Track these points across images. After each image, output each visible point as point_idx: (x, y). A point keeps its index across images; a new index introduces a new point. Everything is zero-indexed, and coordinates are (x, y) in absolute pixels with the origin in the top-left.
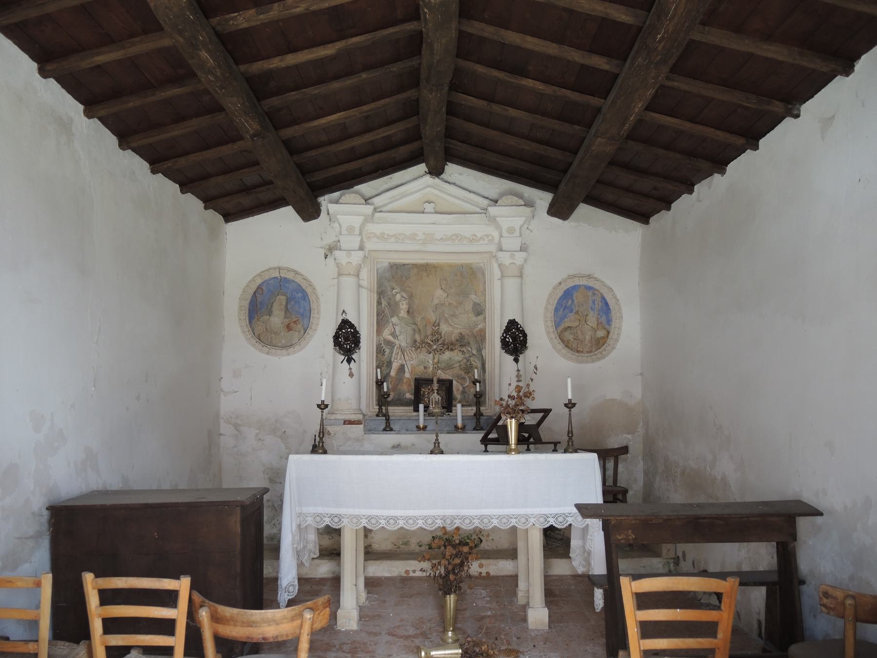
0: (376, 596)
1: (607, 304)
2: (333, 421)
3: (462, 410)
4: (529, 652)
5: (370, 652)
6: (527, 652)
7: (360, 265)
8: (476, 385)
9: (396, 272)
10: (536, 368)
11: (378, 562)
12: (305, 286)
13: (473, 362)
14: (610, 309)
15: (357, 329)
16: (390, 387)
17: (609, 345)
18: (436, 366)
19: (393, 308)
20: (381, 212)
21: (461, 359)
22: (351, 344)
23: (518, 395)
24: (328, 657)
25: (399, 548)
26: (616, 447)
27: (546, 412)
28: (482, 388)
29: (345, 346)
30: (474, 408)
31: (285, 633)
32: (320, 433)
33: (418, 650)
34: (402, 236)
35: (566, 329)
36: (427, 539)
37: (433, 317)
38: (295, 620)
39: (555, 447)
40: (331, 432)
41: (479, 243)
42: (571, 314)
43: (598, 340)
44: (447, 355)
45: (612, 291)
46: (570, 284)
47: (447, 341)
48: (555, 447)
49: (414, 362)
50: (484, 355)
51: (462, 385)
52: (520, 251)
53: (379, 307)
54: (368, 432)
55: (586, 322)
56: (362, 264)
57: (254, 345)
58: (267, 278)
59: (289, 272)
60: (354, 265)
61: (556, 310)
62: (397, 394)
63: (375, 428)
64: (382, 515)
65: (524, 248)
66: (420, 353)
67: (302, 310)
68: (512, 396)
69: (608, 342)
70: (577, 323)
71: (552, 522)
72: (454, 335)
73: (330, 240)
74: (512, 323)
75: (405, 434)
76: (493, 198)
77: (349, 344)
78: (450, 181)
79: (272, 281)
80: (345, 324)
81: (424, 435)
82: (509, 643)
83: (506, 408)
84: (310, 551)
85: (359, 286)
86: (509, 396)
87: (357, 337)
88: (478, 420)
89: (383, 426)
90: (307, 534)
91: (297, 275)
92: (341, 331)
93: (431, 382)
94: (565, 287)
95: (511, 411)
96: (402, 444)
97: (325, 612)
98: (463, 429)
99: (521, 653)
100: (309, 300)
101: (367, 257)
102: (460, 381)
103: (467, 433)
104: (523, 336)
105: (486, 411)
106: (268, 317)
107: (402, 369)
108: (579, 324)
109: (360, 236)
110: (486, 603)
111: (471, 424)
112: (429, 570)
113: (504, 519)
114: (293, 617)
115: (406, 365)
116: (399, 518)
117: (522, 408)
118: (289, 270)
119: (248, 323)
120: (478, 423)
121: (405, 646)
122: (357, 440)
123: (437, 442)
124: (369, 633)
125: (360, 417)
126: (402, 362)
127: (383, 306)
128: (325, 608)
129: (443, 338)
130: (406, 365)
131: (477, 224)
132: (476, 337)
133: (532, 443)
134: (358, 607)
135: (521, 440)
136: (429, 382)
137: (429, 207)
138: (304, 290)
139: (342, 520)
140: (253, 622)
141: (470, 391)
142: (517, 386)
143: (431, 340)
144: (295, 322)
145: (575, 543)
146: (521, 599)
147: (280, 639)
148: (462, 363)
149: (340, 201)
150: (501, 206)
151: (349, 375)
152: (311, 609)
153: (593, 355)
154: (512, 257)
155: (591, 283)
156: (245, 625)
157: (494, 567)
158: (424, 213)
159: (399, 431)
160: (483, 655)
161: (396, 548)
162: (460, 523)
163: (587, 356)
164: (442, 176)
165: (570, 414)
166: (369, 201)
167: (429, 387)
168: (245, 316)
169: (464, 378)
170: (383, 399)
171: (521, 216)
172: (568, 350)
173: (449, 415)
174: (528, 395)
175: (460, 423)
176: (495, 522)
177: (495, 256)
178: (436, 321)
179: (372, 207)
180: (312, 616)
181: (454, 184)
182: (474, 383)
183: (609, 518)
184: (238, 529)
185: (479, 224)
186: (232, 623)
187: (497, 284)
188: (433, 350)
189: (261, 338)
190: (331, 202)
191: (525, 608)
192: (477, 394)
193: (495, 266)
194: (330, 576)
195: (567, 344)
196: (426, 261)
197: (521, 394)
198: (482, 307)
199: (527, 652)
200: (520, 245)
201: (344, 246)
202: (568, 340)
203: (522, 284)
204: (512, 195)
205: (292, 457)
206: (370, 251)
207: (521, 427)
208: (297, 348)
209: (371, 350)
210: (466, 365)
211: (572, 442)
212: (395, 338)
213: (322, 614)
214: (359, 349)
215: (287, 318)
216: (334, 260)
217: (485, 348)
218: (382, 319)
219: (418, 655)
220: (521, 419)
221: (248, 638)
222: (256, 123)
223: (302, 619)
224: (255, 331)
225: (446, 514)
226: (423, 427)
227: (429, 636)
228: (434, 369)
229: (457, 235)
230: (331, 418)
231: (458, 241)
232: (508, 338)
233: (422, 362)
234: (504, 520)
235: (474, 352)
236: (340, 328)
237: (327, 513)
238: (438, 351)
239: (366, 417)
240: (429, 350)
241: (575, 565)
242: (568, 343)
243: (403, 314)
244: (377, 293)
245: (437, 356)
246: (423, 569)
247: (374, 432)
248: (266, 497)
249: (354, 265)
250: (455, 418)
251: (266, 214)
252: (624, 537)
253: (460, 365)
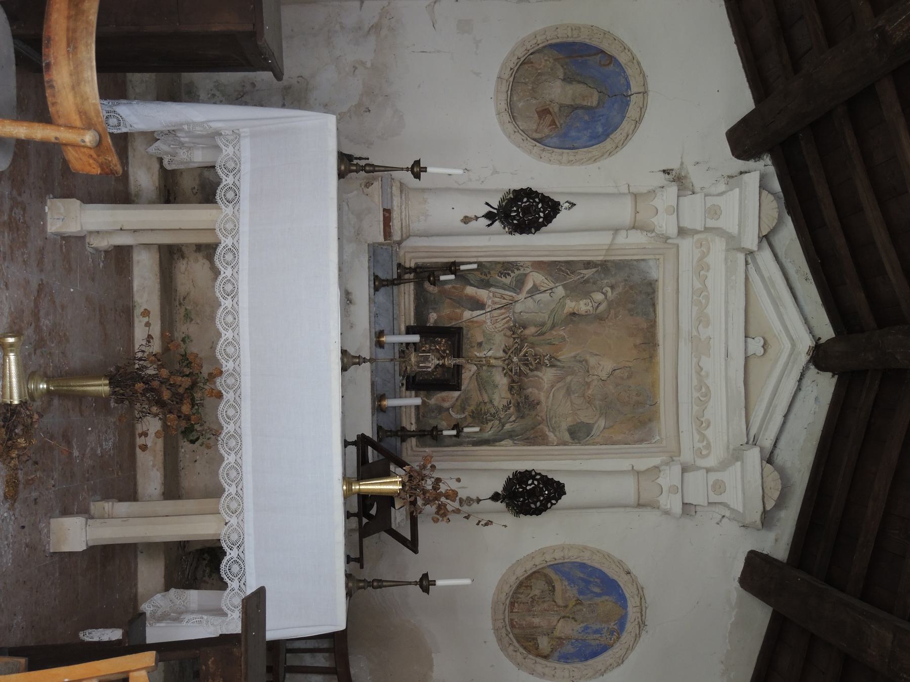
0: (102, 264)
1: (595, 654)
2: (389, 190)
3: (410, 406)
4: (13, 518)
5: (12, 252)
6: (14, 514)
7: (653, 231)
8: (453, 429)
9: (641, 292)
10: (486, 524)
11: (156, 268)
12: (616, 138)
13: (490, 424)
14: (586, 659)
15: (544, 229)
16: (448, 287)
17: (525, 658)
19: (580, 289)
20: (747, 263)
21: (496, 403)
23: (441, 494)
24: (2, 182)
25: (180, 304)
26: (352, 671)
27: (413, 545)
29: (515, 209)
30: (413, 428)
31: (59, 101)
32: (372, 165)
33: (17, 334)
34: (704, 301)
35: (550, 583)
36: (193, 348)
37: (566, 355)
38: (81, 117)
39: (355, 560)
40: (370, 188)
41: (694, 431)
42: (576, 592)
43: (534, 639)
44: (502, 381)
45: (619, 665)
46: (629, 591)
47: (526, 380)
48: (355, 560)
49: (489, 326)
50: (502, 443)
54: (371, 249)
55: (564, 617)
56: (654, 234)
57: (513, 53)
58: (629, 72)
59: (639, 110)
60: (652, 220)
61: (583, 566)
64: (240, 272)
65: (687, 508)
66: (505, 335)
67: (573, 134)
69: (531, 656)
70: (560, 602)
71: (231, 554)
72: (536, 391)
73: (696, 177)
74: (558, 490)
75: (370, 312)
76: (775, 457)
77: (518, 215)
79: (623, 81)
80: (552, 208)
81: (368, 344)
82: (29, 483)
84: (174, 155)
85: (616, 230)
86: (438, 480)
87: (530, 229)
88: (394, 434)
89: (382, 275)
90: (203, 148)
91: (633, 123)
92: (541, 201)
94: (622, 580)
95: (415, 483)
96: (352, 308)
97: (94, 166)
98: (378, 409)
99: (13, 505)
100: (593, 145)
101: (666, 242)
102: (459, 403)
103: (373, 415)
104: (537, 508)
105: (409, 449)
106: (561, 76)
107: (478, 305)
108: (559, 606)
110: (92, 449)
111: (388, 425)
112: (151, 350)
113: (236, 473)
114: (85, 113)
115: (484, 311)
116: (236, 300)
117: (420, 502)
118: (643, 109)
119: (550, 42)
121: (23, 311)
122: (358, 233)
123: (359, 360)
124: (41, 252)
125: (397, 237)
126: (489, 306)
128: (101, 166)
129: (531, 374)
130: (484, 311)
131: (728, 428)
132: (533, 429)
133: (360, 522)
134: (86, 233)
135: (365, 499)
137: (756, 346)
138: (608, 135)
139: (231, 205)
140: (75, 48)
143: (526, 352)
144: (553, 123)
145: (194, 596)
146: (96, 507)
147: (48, 92)
148: (489, 406)
149: (765, 193)
151: (466, 217)
152: (99, 144)
153: (507, 630)
154: (673, 490)
155: (631, 627)
156: (71, 34)
157: (151, 463)
158: (746, 337)
159: (375, 303)
160: (9, 439)
161: (180, 301)
162: (228, 401)
163: (504, 619)
165: (410, 583)
167: (448, 352)
168: (563, 36)
169: (463, 410)
170: (427, 274)
171: (744, 506)
172: (514, 587)
173: (403, 384)
174: (442, 512)
176: (230, 459)
177: (673, 461)
178: (559, 361)
180: (88, 144)
181: (799, 389)
182: (456, 427)
183: (243, 643)
184: (217, 28)
185: (728, 433)
186: (73, 13)
188: (510, 356)
189: (526, 66)
190: (763, 178)
191: (86, 513)
192: (438, 431)
193: (656, 461)
194: (133, 188)
195: (524, 584)
196: (661, 342)
197: (443, 499)
199: (14, 514)
201: (686, 201)
202: (531, 587)
203: (625, 506)
204: (782, 489)
205: (330, 121)
206: (678, 246)
207: (387, 500)
208: (510, 127)
210: (485, 414)
211: (363, 588)
212: (528, 292)
213: (91, 161)
214: (510, 233)
215: (560, 110)
216: (662, 185)
217: (516, 445)
218: (560, 270)
219: (10, 333)
221: (49, 39)
222: (905, 35)
223: (82, 129)
224: (537, 55)
225: (242, 377)
226: (383, 341)
227: (38, 352)
228: (478, 360)
229: (707, 394)
231: (698, 397)
232: (533, 483)
233: (490, 339)
234: (233, 474)
235: (508, 427)
237: (241, 180)
238: (508, 365)
239: (396, 247)
240: (509, 350)
241: (155, 598)
242: (527, 587)
243: (571, 305)
244: (605, 261)
245: (500, 363)
246: (151, 341)
247: (372, 259)
248: (268, 75)
251: (741, 64)
252: (211, 670)
253: (485, 403)
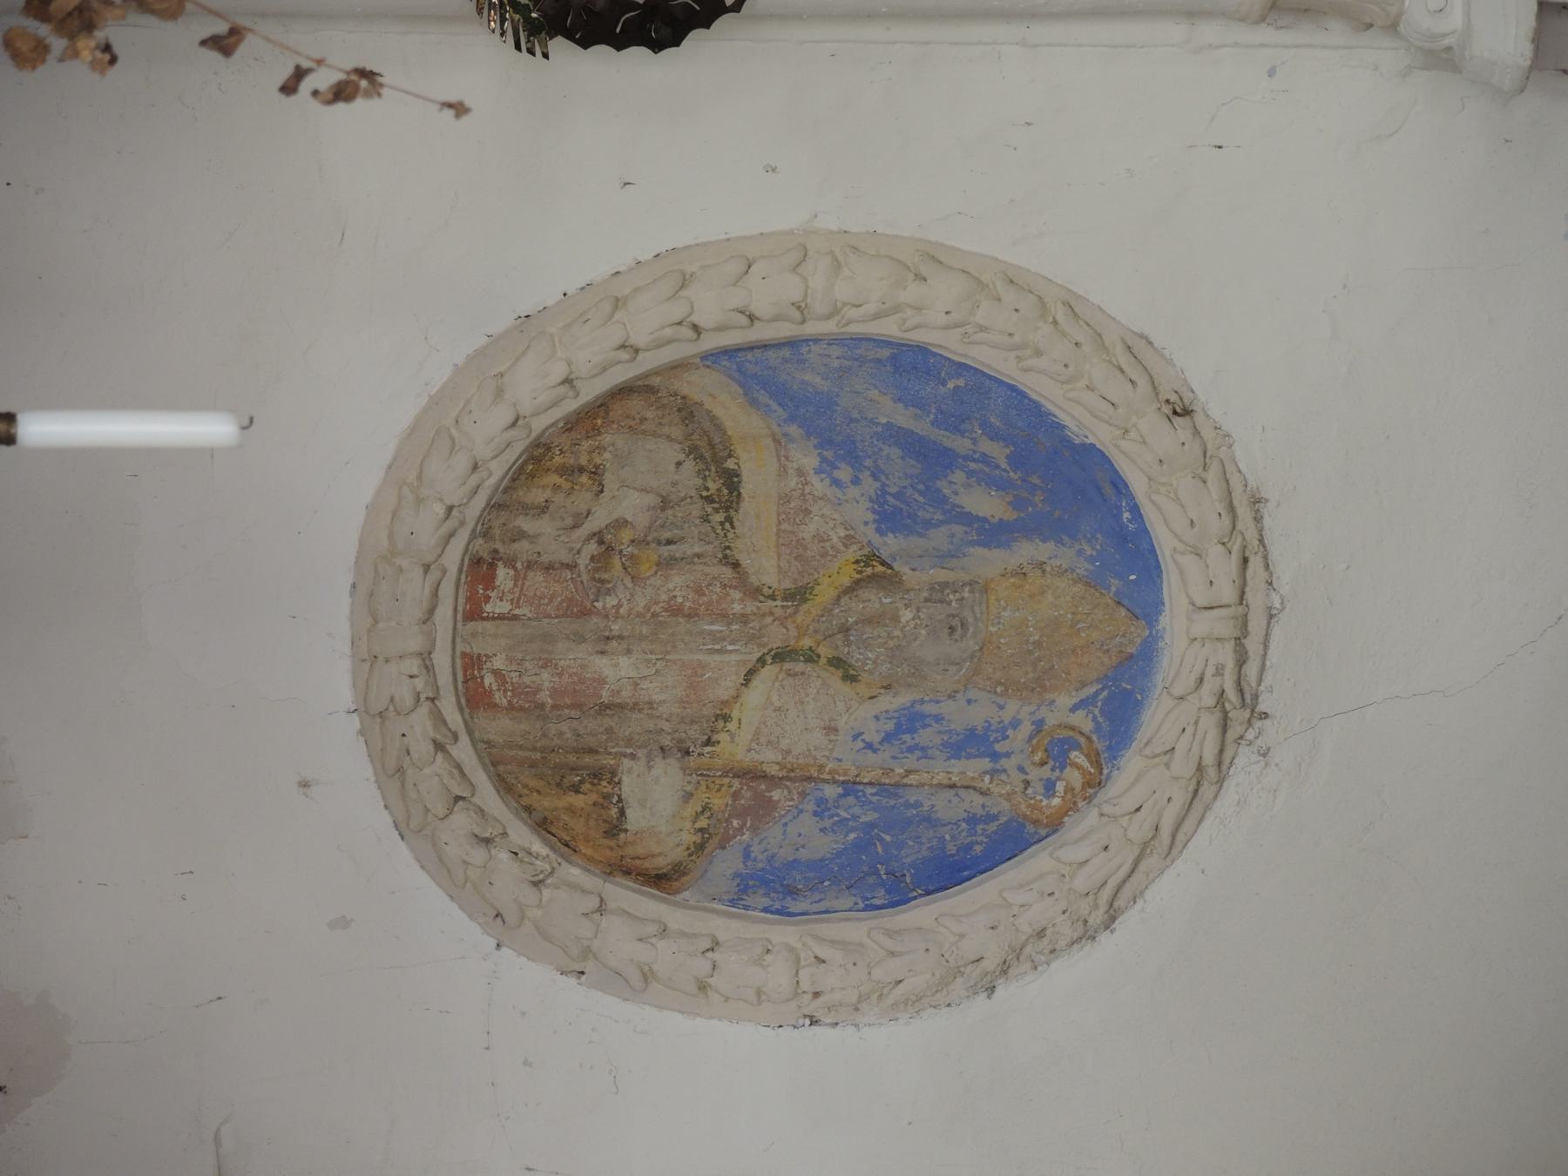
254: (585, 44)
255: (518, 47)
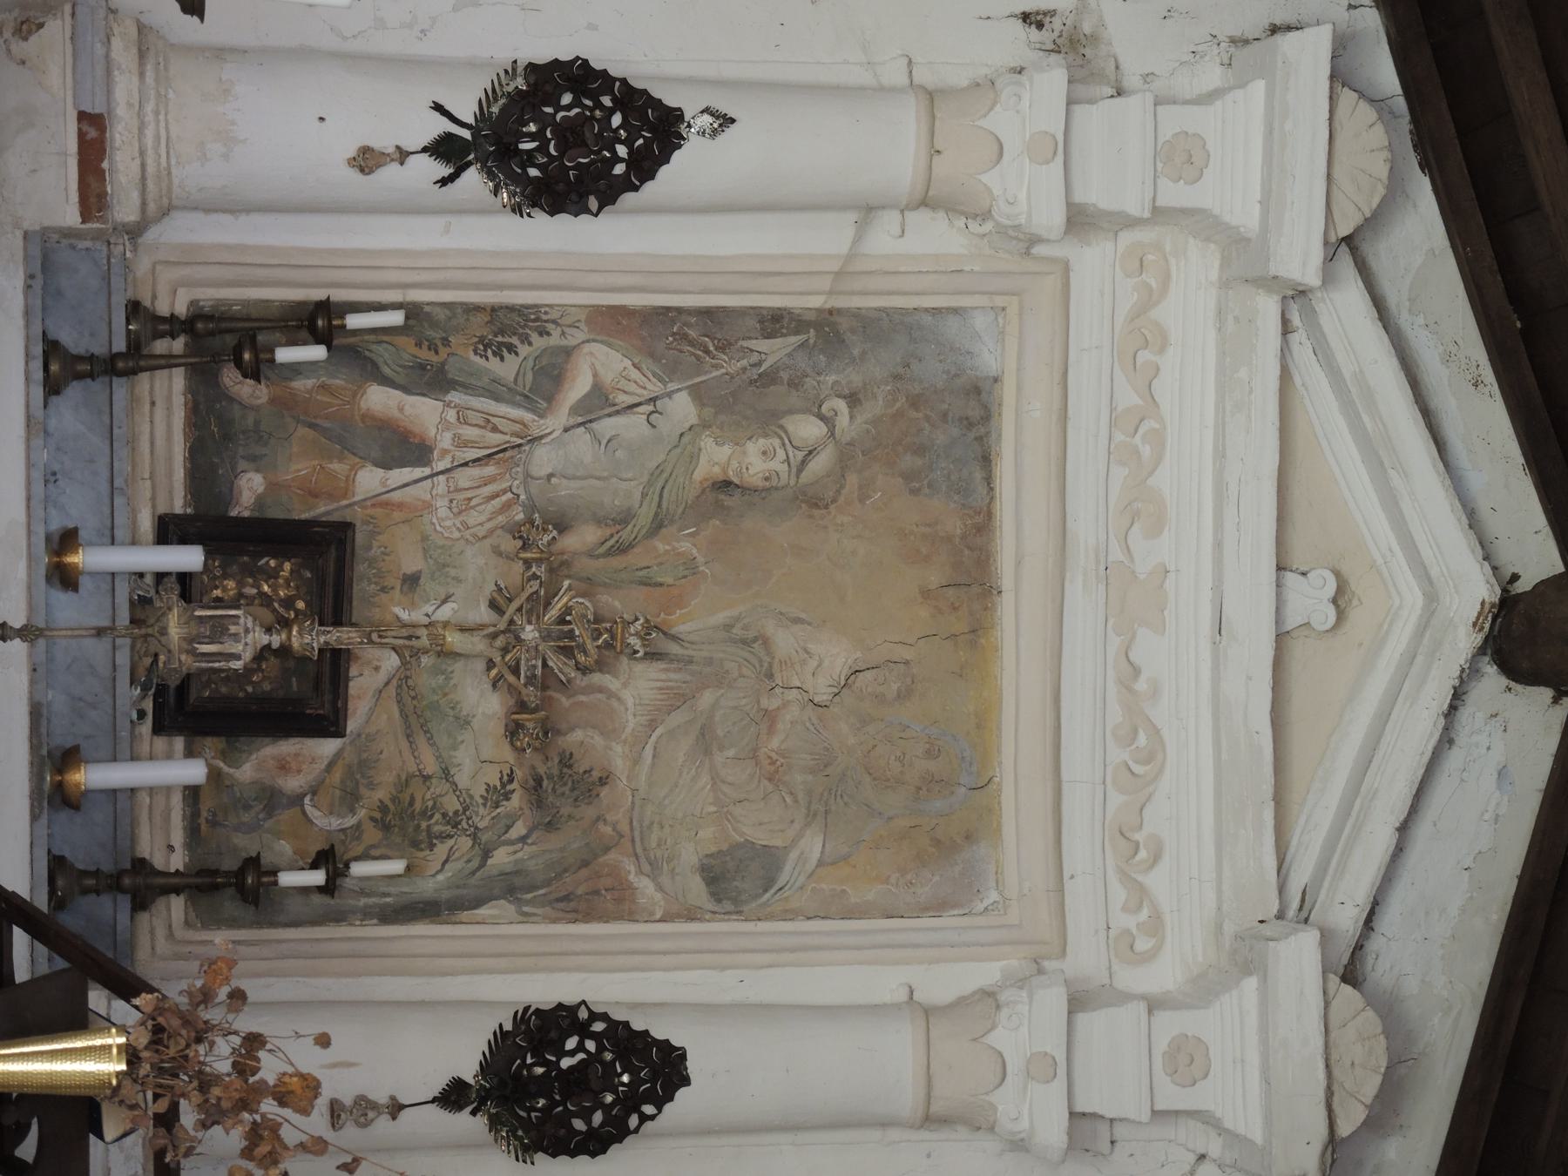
2: (100, 50)
3: (168, 790)
7: (986, 216)
8: (314, 866)
13: (442, 849)
15: (628, 198)
16: (302, 384)
18: (425, 641)
20: (1286, 328)
21: (463, 779)
22: (542, 160)
23: (261, 1090)
28: (295, 906)
29: (532, 128)
30: (177, 862)
34: (1146, 451)
40: (34, 39)
47: (565, 701)
49: (442, 518)
50: (483, 911)
51: (314, 793)
52: (1072, 1114)
53: (752, 323)
54: (36, 252)
56: (988, 226)
60: (985, 178)
62: (257, 423)
63: (59, 293)
66: (498, 552)
68: (258, 1060)
72: (598, 740)
75: (29, 465)
76: (1370, 960)
77: (543, 148)
78: (1464, 715)
83: (186, 1023)
85: (867, 210)
86: (254, 1042)
87: (583, 197)
88: (111, 883)
92: (619, 104)
93: (328, 610)
95: (172, 1052)
102: (337, 776)
103: (34, 818)
104: (591, 1133)
105: (161, 933)
109: (1147, 214)
115: (427, 471)
117: (188, 1117)
120: (91, 882)
125: (125, 209)
126: (445, 452)
127: (752, 344)
129: (581, 681)
130: (427, 471)
132: (585, 864)
136: (329, 601)
141: (279, 835)
142: (312, 1086)
143: (568, 610)
148: (439, 787)
149: (1347, 97)
150: (1327, 1004)
151: (365, 151)
154: (1040, 1068)
164: (1490, 670)
166: (1345, 261)
167: (301, 605)
170: (230, 340)
173: (142, 714)
175: (92, 776)
177: (1041, 971)
178: (675, 638)
179: (1312, 278)
181: (1446, 740)
182: (325, 858)
187: (886, 984)
188: (511, 622)
190: (1342, 47)
193: (985, 973)
196: (1007, 582)
197: (268, 1106)
198: (758, 896)
200: (1109, 1115)
201: (1095, 118)
203: (885, 1124)
206: (1066, 268)
209: (510, 277)
210: (426, 814)
212: (574, 410)
214: (517, 209)
217: (526, 918)
220: (126, 1113)
226: (75, 566)
228: (405, 632)
229: (1154, 755)
230: (116, 43)
232: (580, 1047)
235: (501, 858)
236: (633, 99)
238: (505, 650)
239: (121, 246)
240: (510, 600)
243: (715, 457)
244: (831, 312)
245: (477, 644)
247: (38, 283)
249: (985, 178)
250: (124, 747)
253: (427, 778)
254: (554, 1155)
255: (517, 1160)
